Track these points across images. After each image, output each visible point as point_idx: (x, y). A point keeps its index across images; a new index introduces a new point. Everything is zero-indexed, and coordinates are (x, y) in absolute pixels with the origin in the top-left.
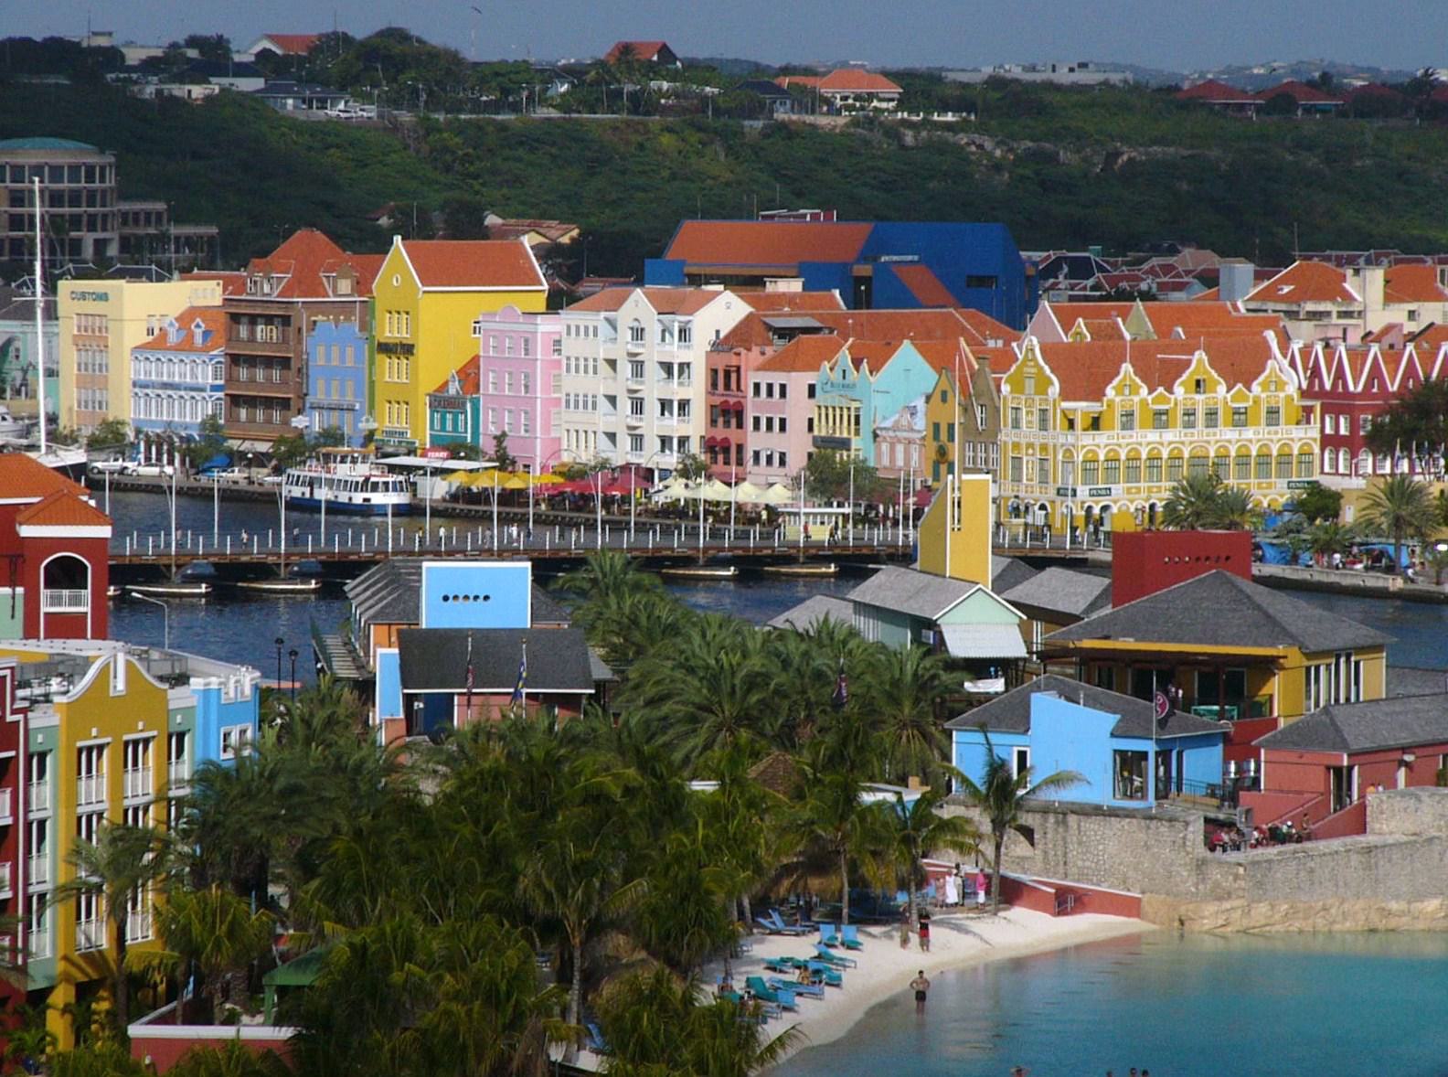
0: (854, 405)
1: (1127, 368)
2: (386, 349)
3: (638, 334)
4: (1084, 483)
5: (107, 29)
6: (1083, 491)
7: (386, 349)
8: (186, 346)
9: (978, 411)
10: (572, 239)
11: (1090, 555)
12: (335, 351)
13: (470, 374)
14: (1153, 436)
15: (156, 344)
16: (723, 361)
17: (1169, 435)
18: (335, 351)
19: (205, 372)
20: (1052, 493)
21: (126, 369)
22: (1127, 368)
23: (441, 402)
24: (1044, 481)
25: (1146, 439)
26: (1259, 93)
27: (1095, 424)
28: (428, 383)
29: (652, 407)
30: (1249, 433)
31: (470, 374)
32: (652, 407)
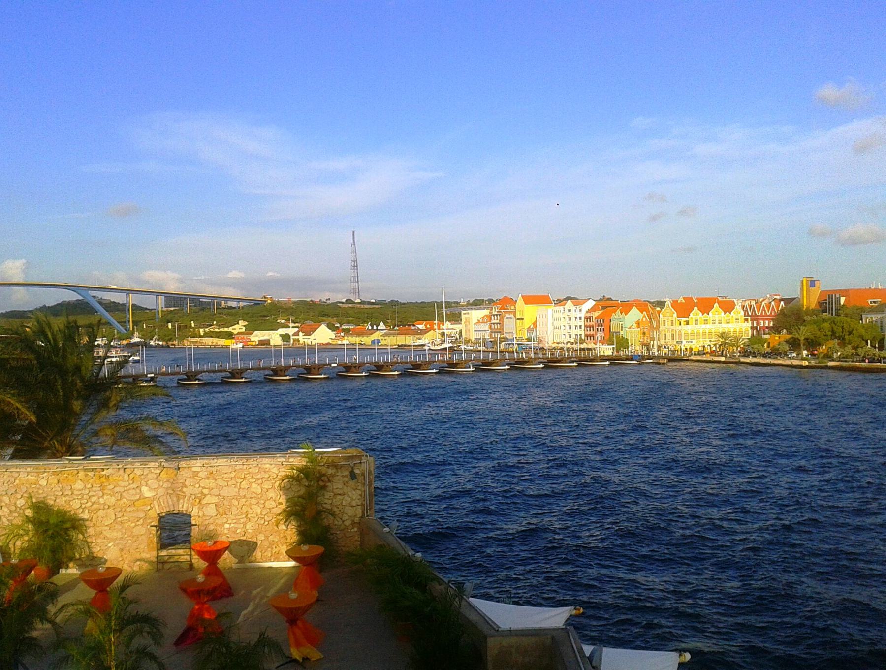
0: (621, 323)
1: (696, 308)
2: (518, 319)
3: (569, 311)
4: (685, 339)
5: (352, 233)
6: (684, 342)
7: (518, 319)
8: (483, 322)
9: (653, 322)
10: (67, 567)
11: (690, 358)
12: (496, 328)
13: (535, 324)
14: (704, 326)
15: (479, 322)
16: (588, 315)
17: (708, 326)
18: (496, 328)
19: (487, 327)
20: (675, 343)
21: (473, 328)
22: (696, 308)
23: (529, 330)
24: (673, 339)
25: (701, 327)
26: (418, 334)
27: (687, 323)
28: (527, 327)
29: (573, 319)
30: (730, 325)
31: (535, 324)
32: (573, 319)
